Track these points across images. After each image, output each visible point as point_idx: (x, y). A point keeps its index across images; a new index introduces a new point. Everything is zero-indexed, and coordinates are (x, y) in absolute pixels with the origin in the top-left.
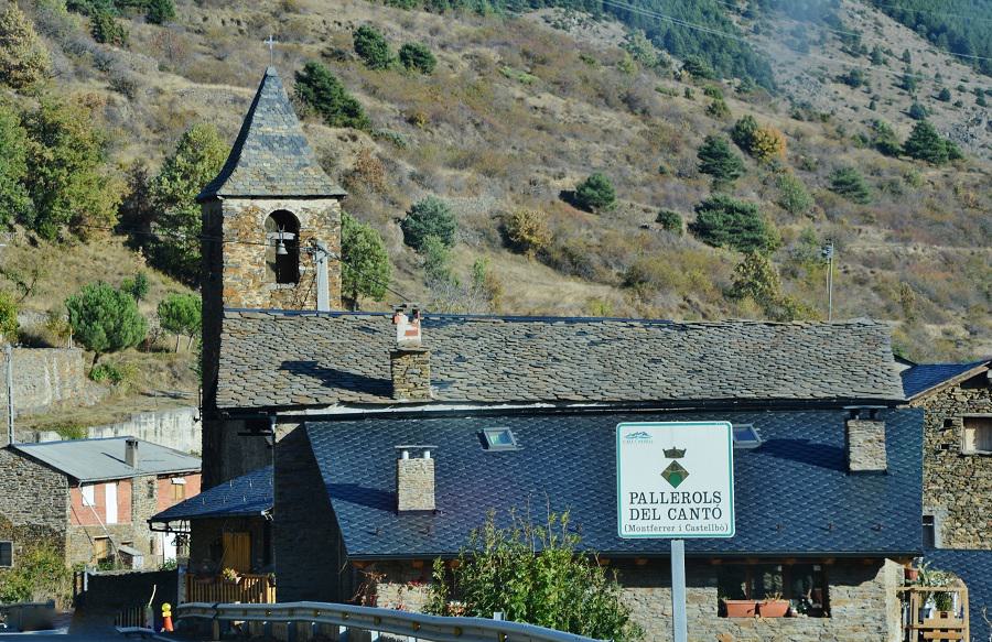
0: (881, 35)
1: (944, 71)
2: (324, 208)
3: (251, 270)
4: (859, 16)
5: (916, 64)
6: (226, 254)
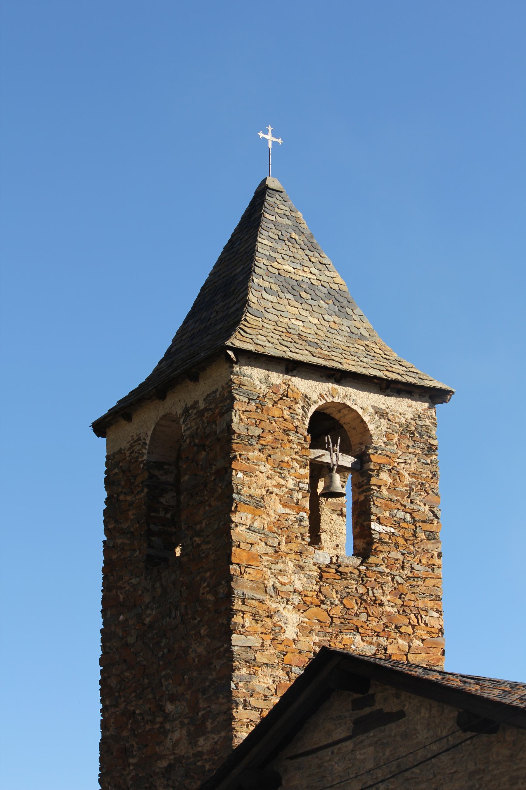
2: (410, 416)
6: (238, 476)
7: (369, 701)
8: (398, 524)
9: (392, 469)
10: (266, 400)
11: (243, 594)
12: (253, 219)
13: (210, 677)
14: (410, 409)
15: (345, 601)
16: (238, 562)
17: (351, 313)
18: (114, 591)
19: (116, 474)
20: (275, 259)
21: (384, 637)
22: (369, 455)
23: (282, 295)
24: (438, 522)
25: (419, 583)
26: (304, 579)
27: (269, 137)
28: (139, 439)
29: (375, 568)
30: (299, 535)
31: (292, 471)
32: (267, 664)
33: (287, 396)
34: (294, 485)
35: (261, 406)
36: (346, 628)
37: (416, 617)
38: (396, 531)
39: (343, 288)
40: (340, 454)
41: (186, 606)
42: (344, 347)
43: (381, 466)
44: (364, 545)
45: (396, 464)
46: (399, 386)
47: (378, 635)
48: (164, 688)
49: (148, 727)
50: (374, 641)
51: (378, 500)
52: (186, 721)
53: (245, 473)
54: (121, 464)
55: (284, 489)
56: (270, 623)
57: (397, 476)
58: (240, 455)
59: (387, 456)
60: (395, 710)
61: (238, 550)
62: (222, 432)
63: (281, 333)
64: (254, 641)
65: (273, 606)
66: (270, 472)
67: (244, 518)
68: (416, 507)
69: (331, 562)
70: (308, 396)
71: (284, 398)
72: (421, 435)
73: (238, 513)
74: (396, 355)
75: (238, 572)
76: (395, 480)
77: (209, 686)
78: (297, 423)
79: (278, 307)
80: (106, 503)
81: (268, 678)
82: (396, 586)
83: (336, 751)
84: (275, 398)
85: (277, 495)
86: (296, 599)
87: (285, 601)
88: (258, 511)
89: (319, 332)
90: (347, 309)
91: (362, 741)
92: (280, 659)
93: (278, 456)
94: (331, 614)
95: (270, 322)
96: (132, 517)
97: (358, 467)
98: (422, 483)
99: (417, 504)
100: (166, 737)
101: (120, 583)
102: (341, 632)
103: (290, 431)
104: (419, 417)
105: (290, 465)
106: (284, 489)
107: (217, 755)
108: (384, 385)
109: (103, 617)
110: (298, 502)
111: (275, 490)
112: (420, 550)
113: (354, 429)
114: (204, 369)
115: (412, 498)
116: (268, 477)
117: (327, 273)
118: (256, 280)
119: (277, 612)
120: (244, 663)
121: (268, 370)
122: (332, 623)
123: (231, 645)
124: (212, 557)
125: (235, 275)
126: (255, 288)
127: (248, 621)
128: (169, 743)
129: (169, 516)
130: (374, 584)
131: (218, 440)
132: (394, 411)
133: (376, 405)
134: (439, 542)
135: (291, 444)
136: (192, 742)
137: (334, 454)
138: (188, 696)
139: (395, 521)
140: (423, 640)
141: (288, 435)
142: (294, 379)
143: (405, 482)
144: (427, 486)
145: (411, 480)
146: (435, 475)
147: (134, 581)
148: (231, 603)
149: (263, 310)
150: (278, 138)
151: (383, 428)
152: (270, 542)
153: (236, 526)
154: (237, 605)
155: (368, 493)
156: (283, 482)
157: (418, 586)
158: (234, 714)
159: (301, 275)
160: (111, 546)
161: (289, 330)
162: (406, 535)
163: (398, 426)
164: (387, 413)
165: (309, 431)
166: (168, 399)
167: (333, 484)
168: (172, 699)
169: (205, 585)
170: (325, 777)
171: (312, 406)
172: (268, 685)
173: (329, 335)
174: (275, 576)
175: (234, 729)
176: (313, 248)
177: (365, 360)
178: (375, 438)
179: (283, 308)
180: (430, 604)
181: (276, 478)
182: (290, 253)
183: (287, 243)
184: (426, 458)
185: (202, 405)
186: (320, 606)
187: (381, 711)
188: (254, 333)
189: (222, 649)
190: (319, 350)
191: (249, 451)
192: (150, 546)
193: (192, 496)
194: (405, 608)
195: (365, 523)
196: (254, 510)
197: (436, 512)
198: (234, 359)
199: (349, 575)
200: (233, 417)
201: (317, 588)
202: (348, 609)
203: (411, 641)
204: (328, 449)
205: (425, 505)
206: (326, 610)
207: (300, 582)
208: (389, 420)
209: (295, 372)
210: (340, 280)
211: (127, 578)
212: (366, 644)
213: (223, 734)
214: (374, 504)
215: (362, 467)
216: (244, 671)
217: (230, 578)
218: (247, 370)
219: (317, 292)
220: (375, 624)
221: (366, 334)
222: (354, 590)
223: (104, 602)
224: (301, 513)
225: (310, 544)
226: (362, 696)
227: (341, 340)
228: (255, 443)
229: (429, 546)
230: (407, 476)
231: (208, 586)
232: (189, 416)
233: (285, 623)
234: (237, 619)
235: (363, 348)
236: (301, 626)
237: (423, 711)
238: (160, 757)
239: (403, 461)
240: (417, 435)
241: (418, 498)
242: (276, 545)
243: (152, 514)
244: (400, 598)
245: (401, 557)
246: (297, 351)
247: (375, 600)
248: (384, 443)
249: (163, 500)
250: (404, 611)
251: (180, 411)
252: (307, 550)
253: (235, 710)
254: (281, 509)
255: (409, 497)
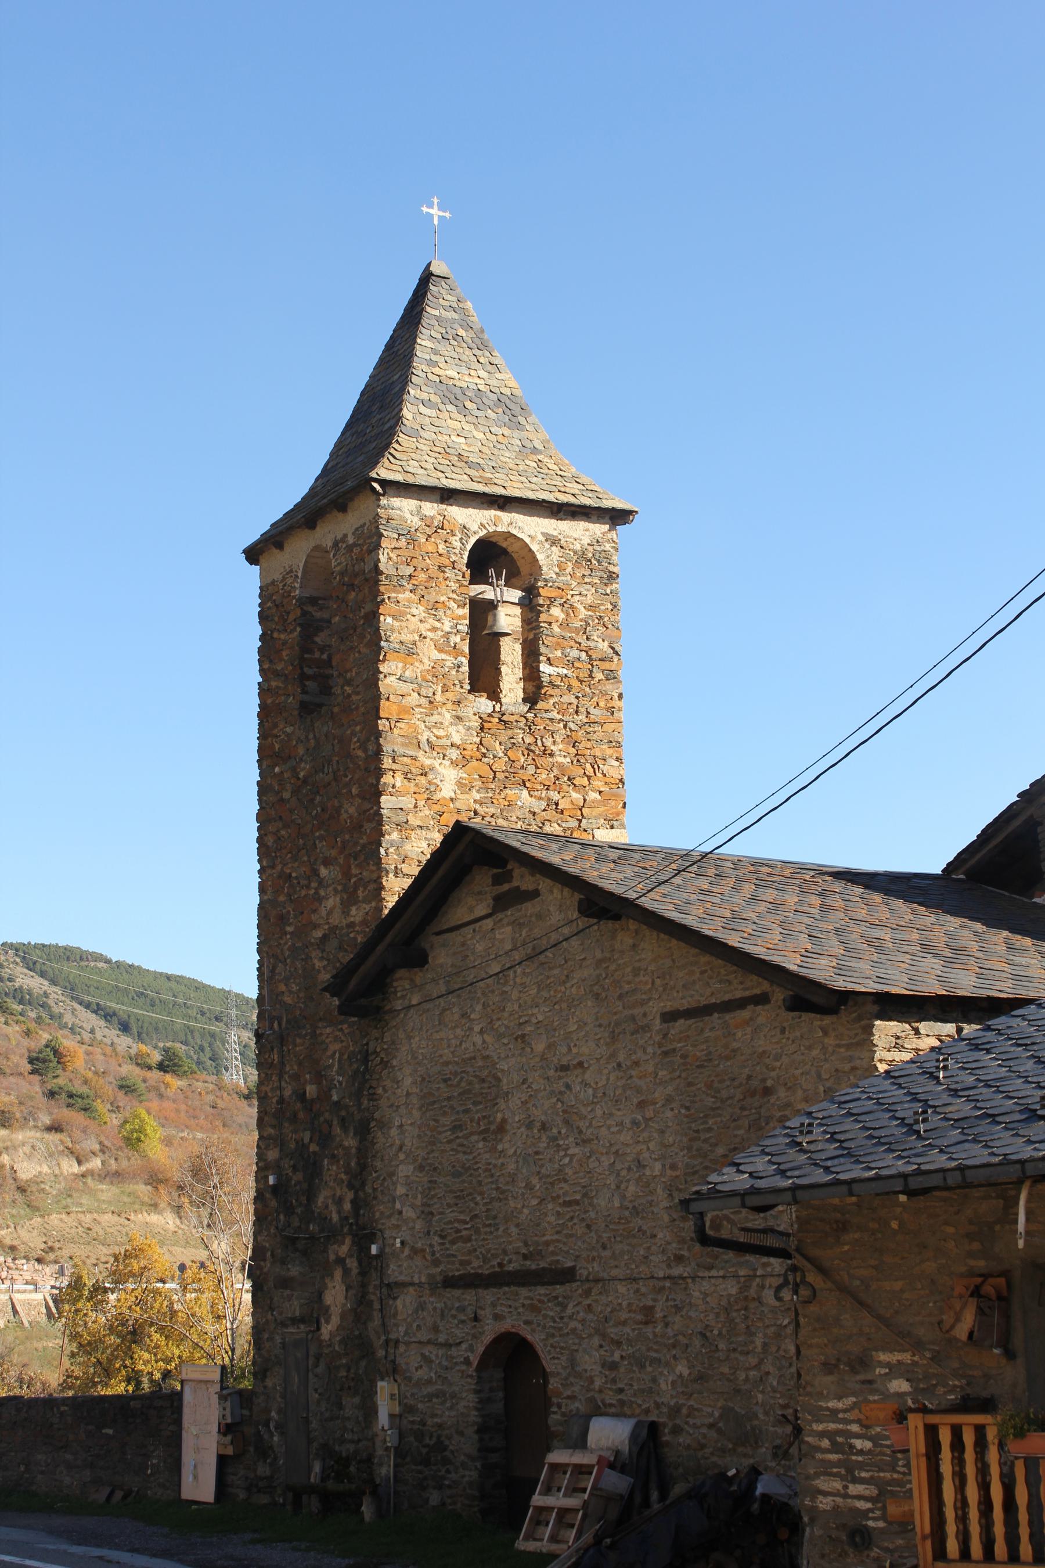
0: (76, 1017)
1: (116, 1040)
2: (586, 541)
3: (437, 664)
4: (62, 1004)
5: (99, 1035)
6: (387, 621)
7: (507, 877)
8: (571, 664)
9: (565, 602)
10: (418, 534)
11: (393, 751)
12: (415, 312)
13: (361, 841)
14: (587, 533)
15: (509, 753)
16: (387, 716)
17: (525, 423)
18: (270, 739)
19: (269, 608)
20: (436, 364)
21: (555, 790)
22: (538, 588)
23: (442, 406)
24: (619, 659)
25: (596, 729)
26: (463, 731)
27: (435, 211)
28: (291, 571)
29: (545, 715)
30: (457, 682)
31: (449, 612)
32: (421, 827)
33: (442, 529)
34: (452, 628)
35: (412, 541)
36: (511, 782)
37: (593, 767)
38: (570, 672)
39: (516, 392)
40: (506, 588)
41: (338, 761)
42: (511, 466)
43: (552, 600)
44: (534, 689)
45: (569, 597)
46: (573, 508)
47: (547, 789)
48: (318, 850)
49: (303, 893)
50: (543, 795)
51: (548, 638)
52: (340, 888)
53: (394, 618)
54: (274, 598)
55: (440, 633)
56: (424, 782)
57: (570, 611)
58: (389, 598)
59: (559, 588)
60: (531, 888)
61: (388, 703)
62: (370, 571)
63: (437, 455)
64: (407, 802)
65: (428, 762)
66: (424, 614)
67: (393, 668)
68: (592, 644)
69: (494, 711)
70: (467, 527)
71: (439, 531)
72: (599, 561)
73: (387, 662)
74: (574, 470)
75: (387, 728)
76: (568, 615)
77: (360, 851)
78: (454, 558)
79: (437, 422)
80: (260, 640)
81: (423, 842)
82: (569, 733)
83: (477, 929)
84: (429, 531)
85: (431, 639)
86: (454, 754)
87: (442, 756)
88: (409, 659)
89: (485, 450)
90: (519, 417)
91: (501, 920)
92: (435, 821)
93: (432, 596)
94: (493, 768)
95: (426, 442)
96: (286, 658)
97: (527, 602)
98: (601, 617)
99: (593, 640)
100: (321, 904)
101: (275, 731)
102: (505, 788)
103: (445, 567)
104: (598, 541)
105: (446, 606)
106: (440, 633)
107: (368, 927)
108: (555, 509)
109: (260, 767)
110: (455, 646)
111: (429, 634)
112: (597, 692)
113: (523, 558)
114: (352, 499)
115: (588, 633)
116: (421, 621)
117: (498, 375)
118: (412, 392)
119: (432, 769)
120: (395, 826)
121: (421, 501)
122: (494, 778)
123: (380, 807)
124: (362, 709)
125: (393, 382)
126: (411, 402)
127: (399, 781)
128: (323, 912)
129: (325, 656)
130: (543, 732)
131: (367, 580)
132: (568, 537)
133: (546, 531)
134: (621, 682)
135: (447, 582)
136: (346, 913)
137: (498, 589)
138: (341, 861)
139: (568, 661)
140: (600, 792)
141: (444, 572)
142: (449, 508)
143: (580, 617)
144: (606, 619)
145: (587, 613)
146: (615, 606)
147: (289, 730)
148: (380, 761)
149: (419, 428)
150: (446, 212)
151: (555, 558)
152: (424, 692)
153: (385, 676)
154: (387, 763)
155: (537, 631)
156: (438, 625)
157: (595, 732)
158: (384, 883)
159: (467, 381)
160: (266, 688)
161: (448, 450)
162: (581, 676)
163: (572, 554)
164: (560, 540)
165: (468, 566)
166: (318, 528)
167: (497, 623)
168: (326, 863)
169: (355, 739)
170: (468, 956)
171: (471, 538)
172: (421, 850)
173: (495, 451)
174: (430, 729)
175: (384, 899)
176: (483, 346)
177: (534, 480)
178: (545, 569)
179: (443, 424)
180: (609, 752)
181: (431, 621)
182: (455, 355)
183: (453, 342)
184: (605, 587)
185: (351, 540)
186: (481, 760)
187: (518, 888)
188: (405, 459)
189: (372, 811)
190: (481, 471)
191: (400, 592)
192: (304, 692)
193: (342, 640)
194: (579, 757)
195: (534, 665)
196: (406, 658)
197: (616, 648)
198: (381, 491)
199: (515, 723)
200: (381, 556)
201: (478, 740)
202: (514, 761)
203: (587, 793)
204: (491, 584)
205: (603, 641)
206: (488, 764)
207: (458, 734)
208: (562, 547)
209: (451, 501)
210: (513, 383)
211: (281, 726)
212: (534, 800)
213: (373, 904)
214: (543, 643)
215: (531, 600)
216: (395, 836)
217: (378, 734)
218: (396, 502)
219: (485, 400)
220: (544, 776)
221: (540, 447)
222: (520, 740)
223: (261, 750)
224: (460, 658)
225: (470, 692)
226: (501, 870)
227: (507, 457)
228: (405, 584)
229: (609, 687)
230: (583, 609)
231: (358, 741)
232: (339, 550)
233: (441, 781)
234: (387, 779)
235: (535, 465)
236: (460, 784)
237: (555, 891)
238: (316, 926)
239: (578, 593)
240: (594, 562)
241: (595, 634)
242: (430, 695)
243: (306, 656)
244: (573, 747)
245: (575, 701)
246: (454, 476)
247: (545, 750)
248: (556, 573)
249: (317, 639)
250: (578, 761)
251: (330, 544)
252: (466, 698)
253: (385, 879)
254: (436, 655)
255: (585, 633)
